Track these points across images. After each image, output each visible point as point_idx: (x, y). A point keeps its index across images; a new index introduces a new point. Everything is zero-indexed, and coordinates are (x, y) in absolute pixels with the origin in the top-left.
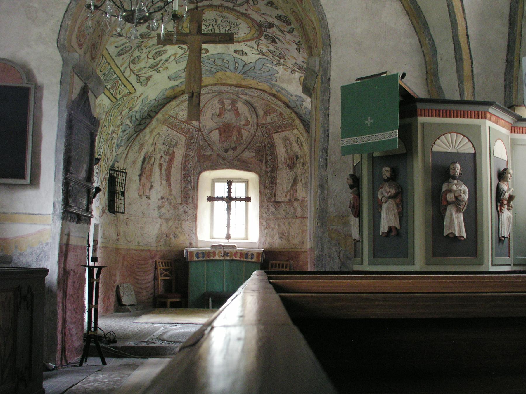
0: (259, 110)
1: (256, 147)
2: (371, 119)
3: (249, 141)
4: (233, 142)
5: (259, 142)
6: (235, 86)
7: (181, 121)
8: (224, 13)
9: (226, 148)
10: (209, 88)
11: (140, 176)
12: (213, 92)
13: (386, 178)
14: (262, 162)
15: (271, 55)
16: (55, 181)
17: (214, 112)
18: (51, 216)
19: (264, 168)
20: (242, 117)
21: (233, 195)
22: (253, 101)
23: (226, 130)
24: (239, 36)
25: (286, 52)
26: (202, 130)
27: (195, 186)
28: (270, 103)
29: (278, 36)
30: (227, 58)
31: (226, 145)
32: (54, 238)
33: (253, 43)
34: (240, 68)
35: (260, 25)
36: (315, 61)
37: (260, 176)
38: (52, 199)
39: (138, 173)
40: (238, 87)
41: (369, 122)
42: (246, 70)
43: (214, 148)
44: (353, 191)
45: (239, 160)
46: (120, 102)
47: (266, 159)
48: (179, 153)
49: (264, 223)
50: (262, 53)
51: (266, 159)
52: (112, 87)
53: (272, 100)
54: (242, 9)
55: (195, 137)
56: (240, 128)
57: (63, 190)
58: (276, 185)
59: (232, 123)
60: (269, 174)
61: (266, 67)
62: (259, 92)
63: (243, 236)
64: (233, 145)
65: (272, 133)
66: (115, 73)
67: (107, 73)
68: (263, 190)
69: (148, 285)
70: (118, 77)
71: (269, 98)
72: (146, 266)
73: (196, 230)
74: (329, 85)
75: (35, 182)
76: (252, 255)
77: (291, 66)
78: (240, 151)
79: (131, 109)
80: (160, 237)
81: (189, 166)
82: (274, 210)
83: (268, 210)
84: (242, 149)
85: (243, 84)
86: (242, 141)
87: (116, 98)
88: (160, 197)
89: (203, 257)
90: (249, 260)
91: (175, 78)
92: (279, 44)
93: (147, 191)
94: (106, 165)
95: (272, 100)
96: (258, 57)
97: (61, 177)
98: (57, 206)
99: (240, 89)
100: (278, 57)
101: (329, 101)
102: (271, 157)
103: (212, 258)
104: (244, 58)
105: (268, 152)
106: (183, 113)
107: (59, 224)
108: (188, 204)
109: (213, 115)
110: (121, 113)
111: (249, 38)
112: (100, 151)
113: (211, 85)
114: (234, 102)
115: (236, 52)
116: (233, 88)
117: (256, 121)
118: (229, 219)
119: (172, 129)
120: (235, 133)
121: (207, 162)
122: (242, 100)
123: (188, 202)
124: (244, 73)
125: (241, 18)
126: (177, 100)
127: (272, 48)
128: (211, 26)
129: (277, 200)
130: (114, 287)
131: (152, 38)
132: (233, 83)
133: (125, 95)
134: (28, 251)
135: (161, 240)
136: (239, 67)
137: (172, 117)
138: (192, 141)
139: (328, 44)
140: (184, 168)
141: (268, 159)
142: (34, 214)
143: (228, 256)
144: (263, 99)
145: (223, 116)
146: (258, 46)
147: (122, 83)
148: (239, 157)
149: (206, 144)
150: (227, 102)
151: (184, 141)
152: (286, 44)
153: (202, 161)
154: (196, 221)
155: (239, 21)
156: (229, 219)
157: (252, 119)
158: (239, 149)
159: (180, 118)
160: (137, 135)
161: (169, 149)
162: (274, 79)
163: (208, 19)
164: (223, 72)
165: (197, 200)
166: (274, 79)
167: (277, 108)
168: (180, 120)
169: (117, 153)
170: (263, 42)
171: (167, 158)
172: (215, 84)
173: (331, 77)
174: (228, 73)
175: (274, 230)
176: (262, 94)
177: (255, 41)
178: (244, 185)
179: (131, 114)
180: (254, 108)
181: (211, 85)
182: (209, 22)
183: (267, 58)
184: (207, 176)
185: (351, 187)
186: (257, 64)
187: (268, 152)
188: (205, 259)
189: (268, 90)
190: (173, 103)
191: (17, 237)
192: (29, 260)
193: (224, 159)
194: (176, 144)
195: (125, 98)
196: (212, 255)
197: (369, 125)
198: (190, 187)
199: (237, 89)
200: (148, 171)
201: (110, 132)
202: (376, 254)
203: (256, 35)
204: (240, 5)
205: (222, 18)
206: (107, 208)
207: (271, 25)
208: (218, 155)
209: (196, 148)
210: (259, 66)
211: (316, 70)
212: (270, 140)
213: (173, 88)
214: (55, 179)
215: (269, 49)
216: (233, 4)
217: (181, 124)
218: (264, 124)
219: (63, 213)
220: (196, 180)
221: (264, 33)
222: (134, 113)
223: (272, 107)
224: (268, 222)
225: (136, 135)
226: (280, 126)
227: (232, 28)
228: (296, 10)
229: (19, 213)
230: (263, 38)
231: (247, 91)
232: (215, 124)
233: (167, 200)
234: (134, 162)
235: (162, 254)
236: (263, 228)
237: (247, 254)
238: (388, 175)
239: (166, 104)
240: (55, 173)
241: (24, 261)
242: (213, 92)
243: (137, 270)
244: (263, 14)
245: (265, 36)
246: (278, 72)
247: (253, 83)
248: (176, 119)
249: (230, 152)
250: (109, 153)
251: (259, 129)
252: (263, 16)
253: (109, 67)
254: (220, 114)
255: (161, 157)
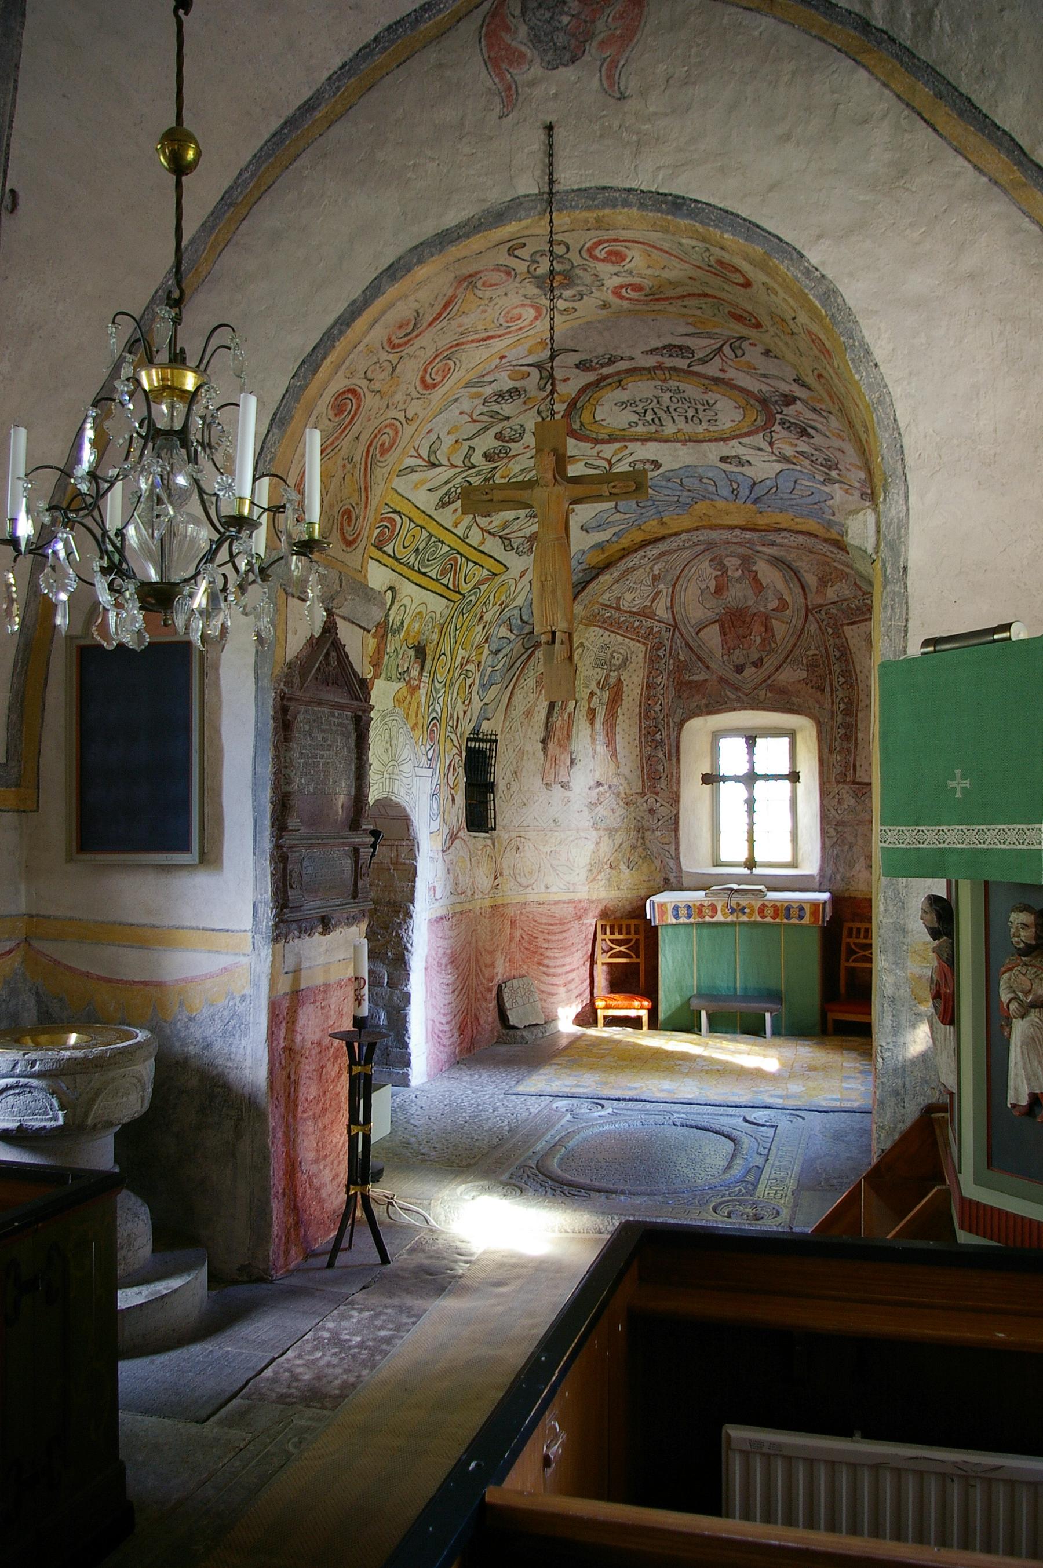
0: (805, 574)
1: (807, 656)
2: (964, 777)
3: (790, 646)
4: (753, 649)
5: (813, 647)
6: (743, 529)
7: (630, 612)
8: (671, 382)
9: (737, 662)
10: (684, 536)
11: (544, 741)
12: (695, 544)
13: (1022, 945)
14: (823, 691)
15: (807, 463)
16: (254, 854)
17: (703, 586)
18: (250, 934)
19: (827, 705)
20: (770, 593)
21: (759, 770)
22: (790, 557)
23: (734, 622)
24: (722, 427)
25: (838, 454)
26: (681, 627)
27: (673, 751)
28: (829, 560)
29: (810, 422)
30: (710, 475)
31: (738, 656)
32: (256, 985)
33: (758, 440)
34: (744, 492)
35: (764, 401)
36: (865, 523)
37: (819, 724)
38: (249, 896)
39: (540, 736)
40: (750, 530)
41: (959, 784)
42: (757, 494)
43: (713, 666)
44: (939, 946)
45: (771, 688)
46: (473, 598)
47: (831, 684)
48: (633, 682)
49: (832, 833)
50: (786, 459)
51: (831, 684)
52: (444, 573)
53: (832, 552)
54: (712, 369)
55: (668, 644)
56: (767, 617)
57: (273, 875)
58: (856, 744)
59: (748, 607)
60: (839, 718)
61: (803, 487)
62: (801, 538)
63: (787, 858)
64: (755, 656)
65: (842, 625)
66: (443, 543)
67: (421, 548)
68: (826, 756)
69: (571, 976)
70: (452, 549)
71: (826, 548)
72: (564, 935)
73: (677, 849)
74: (906, 587)
75: (210, 858)
76: (801, 909)
77: (857, 485)
78: (772, 669)
79: (503, 606)
80: (595, 872)
81: (658, 708)
82: (852, 802)
83: (839, 803)
84: (776, 663)
85: (761, 522)
86: (773, 645)
87: (459, 592)
88: (592, 783)
89: (689, 916)
90: (794, 921)
91: (600, 527)
92: (818, 440)
93: (563, 771)
94: (453, 736)
95: (832, 552)
96: (778, 467)
97: (267, 845)
98: (261, 909)
99: (756, 535)
100: (822, 465)
101: (906, 632)
102: (842, 680)
103: (707, 919)
104: (746, 470)
105: (836, 668)
106: (633, 595)
107: (266, 952)
108: (657, 794)
109: (702, 593)
110: (482, 617)
111: (746, 430)
112: (434, 710)
113: (688, 531)
114: (746, 562)
115: (723, 459)
116: (737, 532)
117: (803, 600)
118: (751, 824)
119: (613, 632)
120: (757, 627)
121: (697, 697)
122: (766, 557)
123: (658, 789)
124: (756, 501)
125: (714, 388)
126: (611, 570)
127: (803, 447)
128: (649, 412)
129: (860, 780)
130: (490, 990)
131: (514, 456)
132: (735, 523)
133: (482, 582)
134: (206, 1012)
135: (599, 877)
136: (741, 489)
137: (610, 606)
138: (661, 653)
139: (900, 472)
140: (646, 713)
141: (835, 683)
142: (213, 930)
143: (744, 913)
144: (811, 552)
145: (725, 593)
146: (771, 444)
147: (468, 560)
148: (769, 681)
149: (694, 658)
150: (732, 563)
151: (641, 655)
152: (834, 438)
153: (685, 695)
154: (676, 830)
155: (711, 397)
156: (751, 824)
157: (793, 596)
158: (770, 663)
159: (625, 605)
160: (530, 657)
161: (608, 676)
162: (829, 511)
163: (637, 399)
164: (708, 502)
165: (678, 782)
166: (829, 511)
167: (847, 570)
168: (626, 612)
169: (485, 701)
170: (779, 436)
171: (606, 695)
172: (697, 529)
173: (910, 565)
174: (720, 504)
175: (854, 849)
176: (809, 541)
177: (761, 435)
178: (786, 741)
179: (507, 613)
180: (796, 573)
181: (688, 531)
182: (641, 405)
183: (798, 468)
184: (698, 728)
185: (935, 934)
186: (780, 480)
187: (836, 668)
188: (692, 920)
189: (821, 532)
190: (605, 578)
191: (182, 980)
192: (209, 1032)
193: (736, 688)
194: (625, 662)
195: (483, 587)
196: (707, 911)
197: (958, 795)
198: (661, 755)
199: (748, 535)
200: (562, 728)
201: (458, 662)
202: (995, 1157)
203: (760, 422)
204: (703, 361)
205: (671, 394)
206: (464, 825)
207: (789, 400)
208: (721, 680)
209: (671, 667)
210: (785, 485)
211: (870, 551)
212: (837, 640)
213: (600, 547)
214: (254, 849)
215: (799, 449)
216: (688, 361)
217: (632, 620)
218: (821, 606)
219: (276, 926)
220: (673, 737)
221: (778, 416)
222: (516, 612)
223: (836, 568)
224: (840, 828)
225: (525, 656)
226: (858, 608)
227: (700, 411)
228: (825, 374)
229: (182, 928)
230: (777, 427)
231: (771, 537)
232: (709, 613)
233: (610, 787)
234: (528, 714)
235: (601, 907)
236: (828, 842)
237: (788, 909)
238: (1026, 936)
239: (588, 582)
240: (255, 836)
241: (198, 1035)
242: (695, 544)
243: (545, 945)
244: (765, 376)
245: (782, 423)
246: (832, 498)
247: (783, 520)
248: (618, 608)
249: (750, 671)
250: (460, 708)
251: (810, 617)
252: (763, 379)
253: (425, 534)
254: (719, 590)
255: (592, 694)
